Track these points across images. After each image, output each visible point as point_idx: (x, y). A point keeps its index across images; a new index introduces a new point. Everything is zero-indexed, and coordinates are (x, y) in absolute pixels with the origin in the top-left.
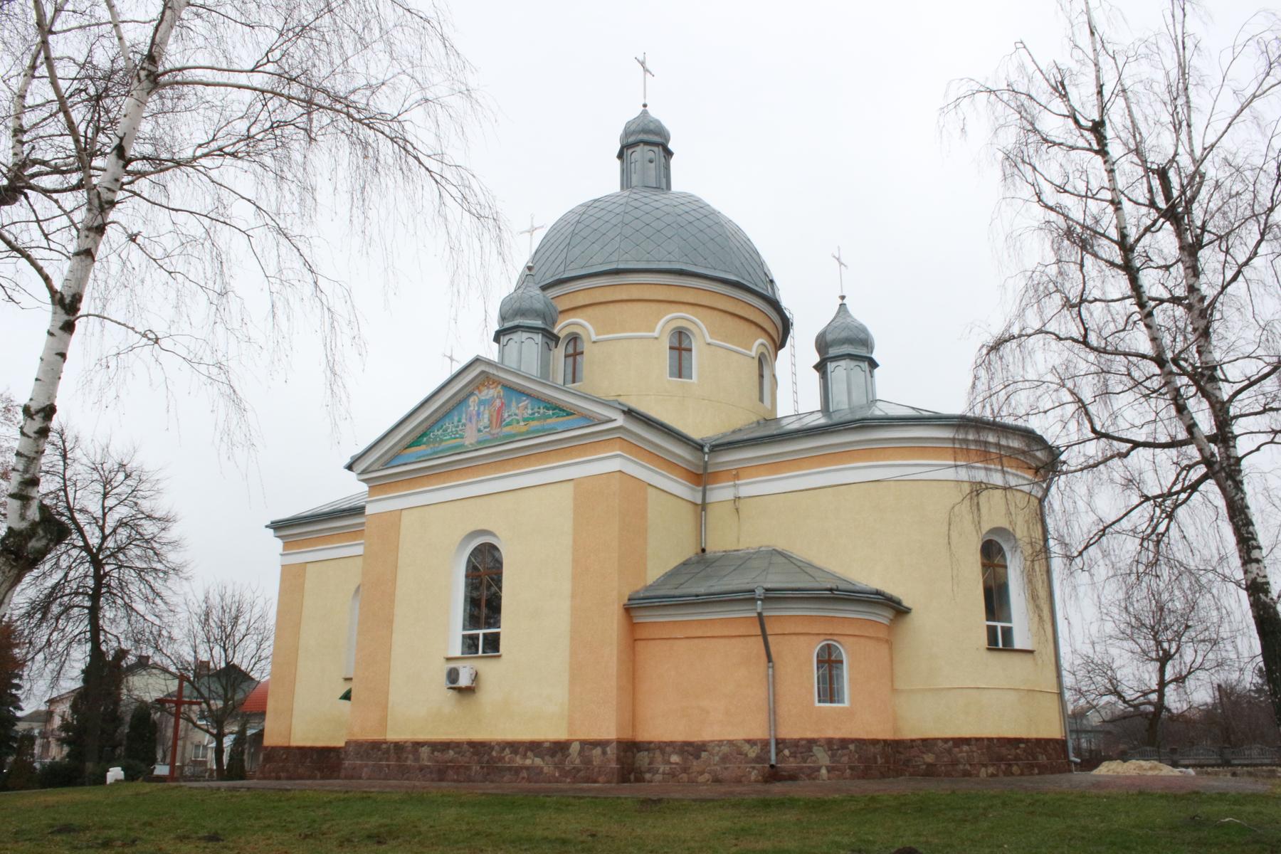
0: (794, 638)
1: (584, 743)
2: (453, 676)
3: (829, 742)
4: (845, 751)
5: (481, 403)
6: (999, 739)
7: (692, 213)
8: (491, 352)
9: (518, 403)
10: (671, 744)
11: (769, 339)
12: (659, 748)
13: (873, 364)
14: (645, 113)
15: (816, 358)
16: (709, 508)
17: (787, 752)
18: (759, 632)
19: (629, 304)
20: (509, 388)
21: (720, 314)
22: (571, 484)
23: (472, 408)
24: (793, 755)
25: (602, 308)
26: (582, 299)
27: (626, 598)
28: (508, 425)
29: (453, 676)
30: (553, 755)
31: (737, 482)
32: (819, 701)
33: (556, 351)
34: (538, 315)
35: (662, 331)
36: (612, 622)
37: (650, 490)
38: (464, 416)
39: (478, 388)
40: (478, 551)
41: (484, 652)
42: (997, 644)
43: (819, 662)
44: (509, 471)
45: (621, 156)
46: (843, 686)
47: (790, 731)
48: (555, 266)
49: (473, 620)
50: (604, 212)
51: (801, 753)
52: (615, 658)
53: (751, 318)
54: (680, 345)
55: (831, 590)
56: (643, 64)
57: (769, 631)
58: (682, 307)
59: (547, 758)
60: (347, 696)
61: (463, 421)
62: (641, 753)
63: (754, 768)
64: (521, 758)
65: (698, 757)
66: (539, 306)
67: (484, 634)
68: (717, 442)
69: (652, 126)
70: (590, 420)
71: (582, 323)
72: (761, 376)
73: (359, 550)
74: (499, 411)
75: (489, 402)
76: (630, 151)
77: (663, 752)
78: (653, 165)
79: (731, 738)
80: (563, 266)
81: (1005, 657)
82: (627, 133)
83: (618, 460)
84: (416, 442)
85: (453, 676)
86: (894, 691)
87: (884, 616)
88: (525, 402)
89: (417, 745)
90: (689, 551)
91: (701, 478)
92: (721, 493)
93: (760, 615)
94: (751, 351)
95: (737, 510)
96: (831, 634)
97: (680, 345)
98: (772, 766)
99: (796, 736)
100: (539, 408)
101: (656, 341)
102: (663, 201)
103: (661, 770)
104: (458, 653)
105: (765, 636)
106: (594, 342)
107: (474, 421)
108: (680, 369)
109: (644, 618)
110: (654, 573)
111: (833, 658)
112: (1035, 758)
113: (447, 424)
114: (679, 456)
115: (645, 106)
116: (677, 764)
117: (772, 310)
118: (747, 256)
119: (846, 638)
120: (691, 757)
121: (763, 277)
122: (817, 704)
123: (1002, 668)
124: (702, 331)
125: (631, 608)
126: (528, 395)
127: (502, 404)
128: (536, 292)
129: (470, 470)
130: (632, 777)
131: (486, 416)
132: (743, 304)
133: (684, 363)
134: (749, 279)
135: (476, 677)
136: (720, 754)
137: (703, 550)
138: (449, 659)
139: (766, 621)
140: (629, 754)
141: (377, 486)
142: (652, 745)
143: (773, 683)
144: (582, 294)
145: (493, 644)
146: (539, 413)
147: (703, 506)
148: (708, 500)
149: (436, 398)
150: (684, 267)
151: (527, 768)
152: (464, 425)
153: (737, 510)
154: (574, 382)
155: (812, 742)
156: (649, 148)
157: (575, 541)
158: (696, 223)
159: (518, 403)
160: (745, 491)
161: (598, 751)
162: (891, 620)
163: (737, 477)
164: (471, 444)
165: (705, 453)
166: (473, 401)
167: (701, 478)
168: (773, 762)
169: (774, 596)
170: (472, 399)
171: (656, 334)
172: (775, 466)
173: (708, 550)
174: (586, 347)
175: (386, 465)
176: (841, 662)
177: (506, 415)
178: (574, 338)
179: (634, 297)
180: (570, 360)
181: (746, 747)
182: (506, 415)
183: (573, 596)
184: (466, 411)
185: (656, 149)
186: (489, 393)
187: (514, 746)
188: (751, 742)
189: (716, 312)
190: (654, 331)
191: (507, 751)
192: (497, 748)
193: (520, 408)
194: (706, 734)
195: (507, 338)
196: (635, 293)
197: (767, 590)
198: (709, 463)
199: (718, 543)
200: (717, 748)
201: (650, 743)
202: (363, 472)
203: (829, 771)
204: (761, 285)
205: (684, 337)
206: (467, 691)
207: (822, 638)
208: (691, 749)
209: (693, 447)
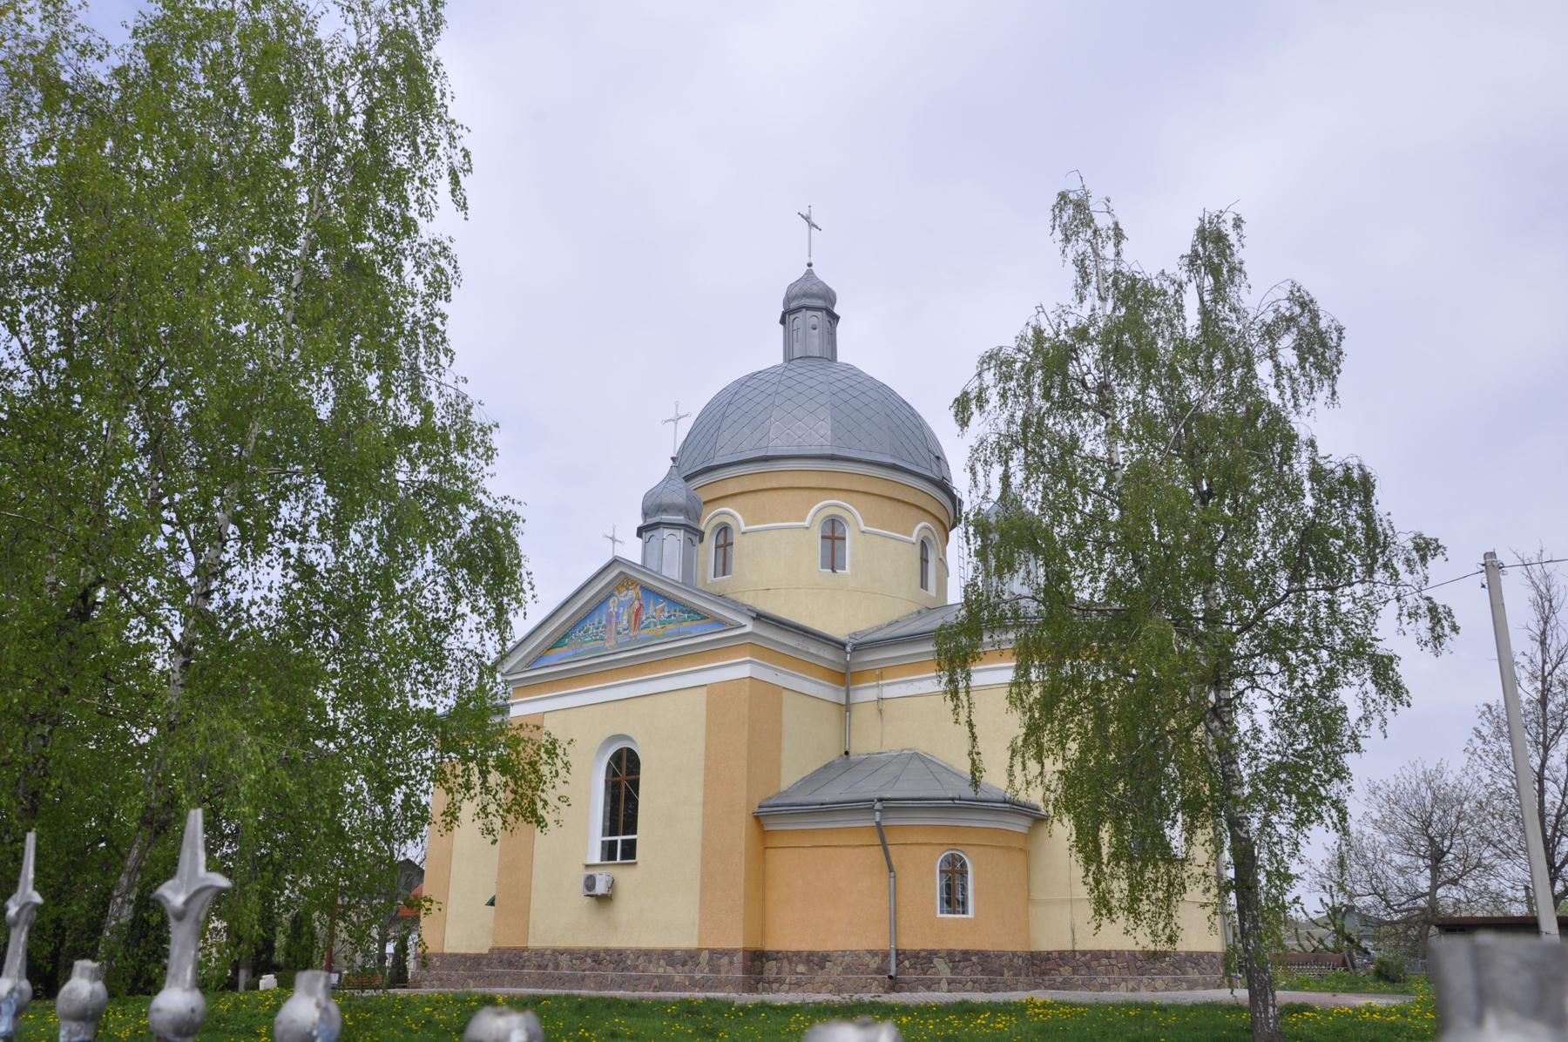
1: (712, 952)
3: (950, 954)
4: (967, 963)
5: (621, 604)
8: (632, 550)
9: (655, 605)
10: (798, 953)
11: (934, 521)
14: (809, 274)
17: (907, 963)
20: (648, 591)
22: (705, 689)
24: (913, 966)
25: (753, 496)
26: (732, 488)
28: (647, 627)
30: (684, 965)
32: (942, 912)
33: (700, 547)
34: (680, 511)
36: (739, 830)
37: (785, 693)
40: (617, 758)
43: (941, 872)
45: (783, 321)
47: (909, 943)
49: (612, 827)
54: (833, 534)
55: (953, 799)
56: (807, 219)
57: (888, 842)
58: (835, 494)
59: (679, 967)
60: (492, 903)
63: (875, 979)
65: (823, 968)
66: (680, 499)
67: (623, 841)
68: (868, 638)
70: (721, 623)
71: (733, 513)
72: (924, 561)
74: (637, 613)
76: (792, 317)
77: (790, 962)
78: (816, 332)
82: (788, 299)
84: (558, 643)
85: (590, 883)
87: (1020, 825)
89: (557, 952)
90: (832, 754)
91: (845, 677)
92: (865, 694)
95: (880, 711)
97: (833, 534)
98: (890, 977)
99: (917, 948)
102: (819, 378)
104: (597, 860)
105: (884, 845)
108: (833, 561)
109: (772, 826)
110: (789, 777)
118: (909, 433)
122: (939, 915)
124: (856, 520)
125: (761, 819)
126: (665, 598)
128: (680, 483)
130: (760, 986)
131: (625, 617)
133: (837, 554)
135: (612, 885)
137: (847, 753)
138: (588, 866)
140: (758, 963)
143: (894, 893)
145: (630, 850)
147: (847, 707)
148: (851, 701)
150: (836, 453)
153: (880, 711)
154: (724, 574)
155: (932, 954)
157: (707, 748)
159: (655, 605)
160: (888, 692)
161: (725, 960)
163: (881, 677)
167: (845, 677)
168: (892, 974)
171: (806, 524)
173: (851, 754)
174: (736, 538)
178: (724, 530)
179: (784, 485)
180: (721, 551)
181: (868, 958)
183: (705, 803)
185: (819, 314)
187: (648, 954)
188: (874, 953)
190: (804, 520)
193: (654, 610)
194: (829, 946)
195: (649, 534)
196: (785, 481)
199: (862, 745)
201: (778, 952)
203: (949, 984)
204: (924, 464)
205: (837, 524)
206: (604, 900)
207: (946, 847)
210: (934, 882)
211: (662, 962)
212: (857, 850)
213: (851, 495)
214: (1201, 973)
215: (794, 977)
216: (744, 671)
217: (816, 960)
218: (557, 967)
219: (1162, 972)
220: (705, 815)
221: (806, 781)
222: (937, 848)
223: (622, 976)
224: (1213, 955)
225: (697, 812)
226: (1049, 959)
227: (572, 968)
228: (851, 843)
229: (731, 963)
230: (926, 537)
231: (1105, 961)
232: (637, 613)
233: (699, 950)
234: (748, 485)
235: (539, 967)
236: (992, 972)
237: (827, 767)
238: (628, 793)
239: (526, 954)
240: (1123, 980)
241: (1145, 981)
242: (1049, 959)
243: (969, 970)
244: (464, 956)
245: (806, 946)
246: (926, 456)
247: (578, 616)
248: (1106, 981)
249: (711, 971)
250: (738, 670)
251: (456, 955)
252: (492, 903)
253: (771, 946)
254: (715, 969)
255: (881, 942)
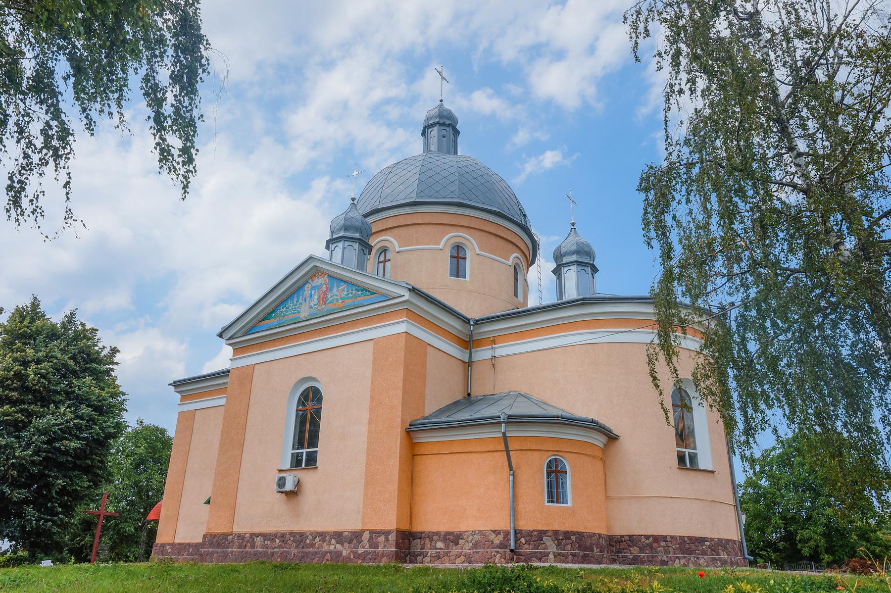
0: (530, 452)
1: (372, 532)
2: (281, 482)
3: (556, 533)
5: (313, 288)
6: (690, 538)
7: (469, 167)
8: (320, 251)
12: (428, 537)
13: (595, 270)
14: (441, 106)
15: (554, 266)
16: (474, 366)
17: (523, 540)
18: (503, 447)
19: (423, 226)
21: (486, 234)
23: (306, 292)
25: (405, 228)
27: (409, 424)
29: (281, 482)
30: (350, 542)
31: (494, 346)
35: (445, 245)
36: (395, 441)
37: (429, 348)
38: (301, 297)
39: (311, 278)
41: (306, 466)
42: (685, 464)
44: (329, 334)
45: (423, 134)
46: (566, 491)
47: (525, 525)
48: (373, 201)
49: (299, 442)
50: (408, 166)
51: (534, 541)
52: (397, 468)
53: (509, 238)
54: (458, 256)
58: (460, 228)
59: (346, 545)
61: (300, 301)
62: (416, 541)
63: (498, 552)
64: (327, 545)
65: (457, 544)
69: (445, 113)
72: (516, 279)
73: (223, 402)
74: (325, 294)
75: (319, 287)
76: (430, 130)
77: (431, 540)
78: (445, 139)
79: (482, 529)
80: (378, 201)
81: (692, 473)
83: (404, 325)
84: (264, 319)
85: (281, 482)
86: (607, 498)
87: (599, 440)
88: (343, 286)
90: (459, 396)
91: (468, 343)
92: (482, 354)
93: (504, 434)
94: (508, 261)
96: (557, 451)
97: (458, 256)
100: (352, 290)
101: (441, 252)
103: (429, 554)
104: (288, 467)
105: (507, 451)
106: (398, 252)
107: (308, 299)
108: (458, 271)
111: (559, 469)
112: (718, 554)
113: (290, 304)
114: (452, 326)
115: (441, 101)
116: (441, 549)
117: (527, 237)
118: (507, 196)
119: (568, 454)
120: (451, 544)
121: (518, 212)
123: (686, 483)
125: (412, 431)
126: (345, 282)
127: (327, 288)
129: (303, 335)
130: (408, 558)
131: (316, 297)
132: (504, 229)
133: (461, 268)
134: (508, 211)
135: (298, 484)
136: (473, 541)
137: (469, 395)
138: (280, 471)
139: (508, 439)
140: (406, 541)
141: (240, 349)
142: (423, 535)
144: (390, 220)
145: (312, 460)
146: (352, 293)
149: (281, 285)
151: (331, 552)
152: (301, 304)
155: (542, 533)
156: (443, 128)
158: (472, 173)
161: (382, 539)
162: (605, 444)
163: (494, 342)
164: (305, 317)
165: (471, 325)
166: (307, 287)
167: (468, 343)
168: (512, 547)
169: (514, 420)
170: (307, 286)
171: (441, 247)
172: (521, 334)
173: (473, 394)
175: (246, 334)
176: (565, 472)
177: (329, 296)
181: (493, 536)
182: (329, 296)
183: (370, 423)
184: (303, 294)
185: (447, 129)
186: (319, 281)
187: (322, 535)
189: (484, 233)
190: (439, 244)
191: (317, 540)
192: (310, 537)
193: (339, 293)
194: (462, 527)
195: (334, 245)
197: (510, 416)
198: (474, 332)
200: (471, 537)
202: (230, 338)
203: (555, 557)
206: (292, 495)
207: (550, 453)
208: (451, 537)
209: (463, 320)
210: (543, 479)
211: (333, 541)
212: (485, 455)
213: (471, 230)
214: (728, 555)
215: (434, 552)
216: (402, 328)
217: (453, 538)
218: (253, 546)
219: (704, 553)
220: (369, 431)
221: (441, 411)
222: (545, 453)
223: (303, 552)
224: (734, 542)
225: (364, 429)
226: (622, 541)
227: (263, 547)
228: (479, 449)
229: (387, 540)
230: (517, 264)
231: (663, 544)
232: (325, 294)
233: (362, 532)
234: (402, 221)
235: (240, 547)
236: (586, 549)
237: (456, 403)
238: (312, 418)
239: (230, 537)
240: (677, 558)
241: (692, 559)
242: (622, 541)
243: (569, 547)
244: (189, 544)
245: (443, 528)
246: (519, 214)
247: (284, 297)
248: (665, 558)
249: (370, 547)
250: (399, 327)
251: (184, 544)
252: (208, 502)
253: (418, 527)
254: (374, 545)
255: (503, 522)
